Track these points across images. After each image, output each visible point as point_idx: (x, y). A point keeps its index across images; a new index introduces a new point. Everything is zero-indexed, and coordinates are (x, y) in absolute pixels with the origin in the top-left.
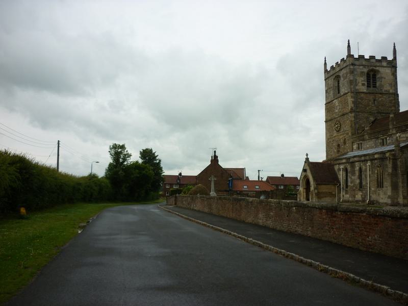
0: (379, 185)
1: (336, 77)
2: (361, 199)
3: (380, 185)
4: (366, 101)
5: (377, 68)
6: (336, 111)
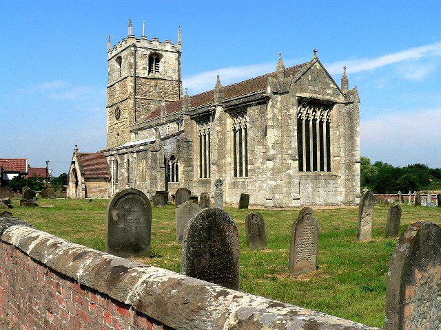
0: (238, 172)
5: (160, 52)
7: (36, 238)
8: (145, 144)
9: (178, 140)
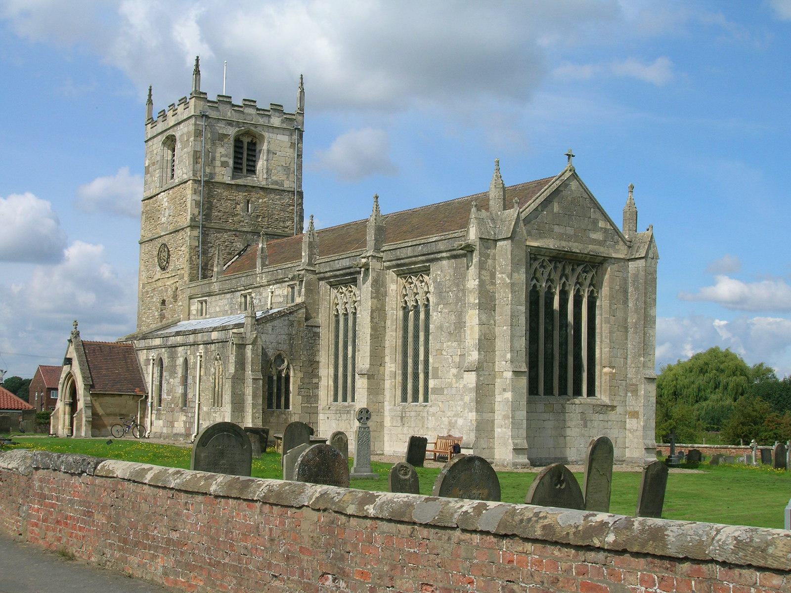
0: (216, 401)
1: (167, 138)
2: (183, 431)
4: (229, 203)
5: (259, 130)
6: (164, 220)
8: (224, 329)
9: (291, 324)
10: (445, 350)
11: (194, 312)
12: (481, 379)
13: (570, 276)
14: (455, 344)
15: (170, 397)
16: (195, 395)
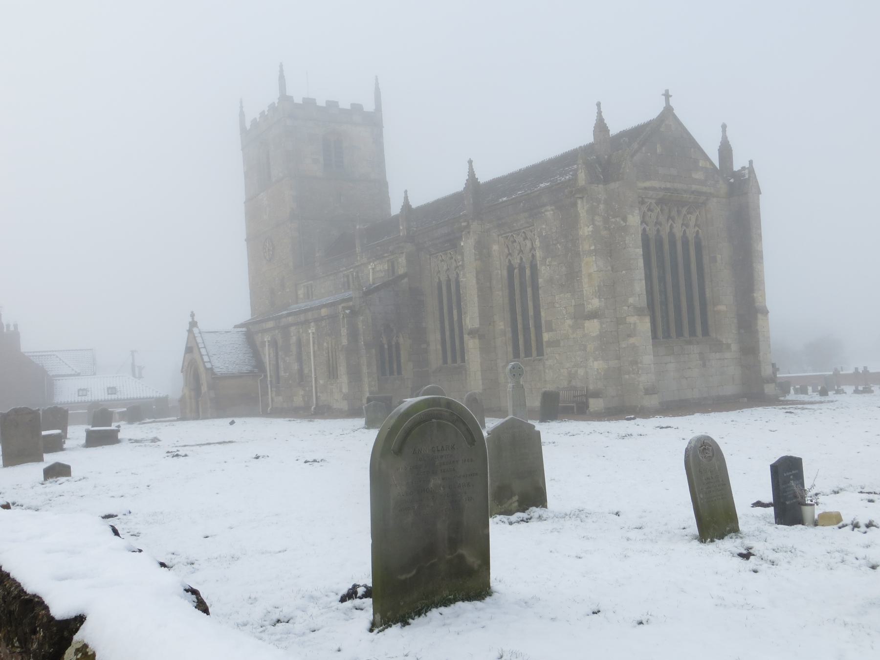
0: (521, 347)
3: (332, 373)
7: (420, 392)
10: (557, 302)
11: (301, 296)
12: (604, 326)
13: (676, 218)
14: (569, 295)
15: (287, 374)
16: (311, 371)
